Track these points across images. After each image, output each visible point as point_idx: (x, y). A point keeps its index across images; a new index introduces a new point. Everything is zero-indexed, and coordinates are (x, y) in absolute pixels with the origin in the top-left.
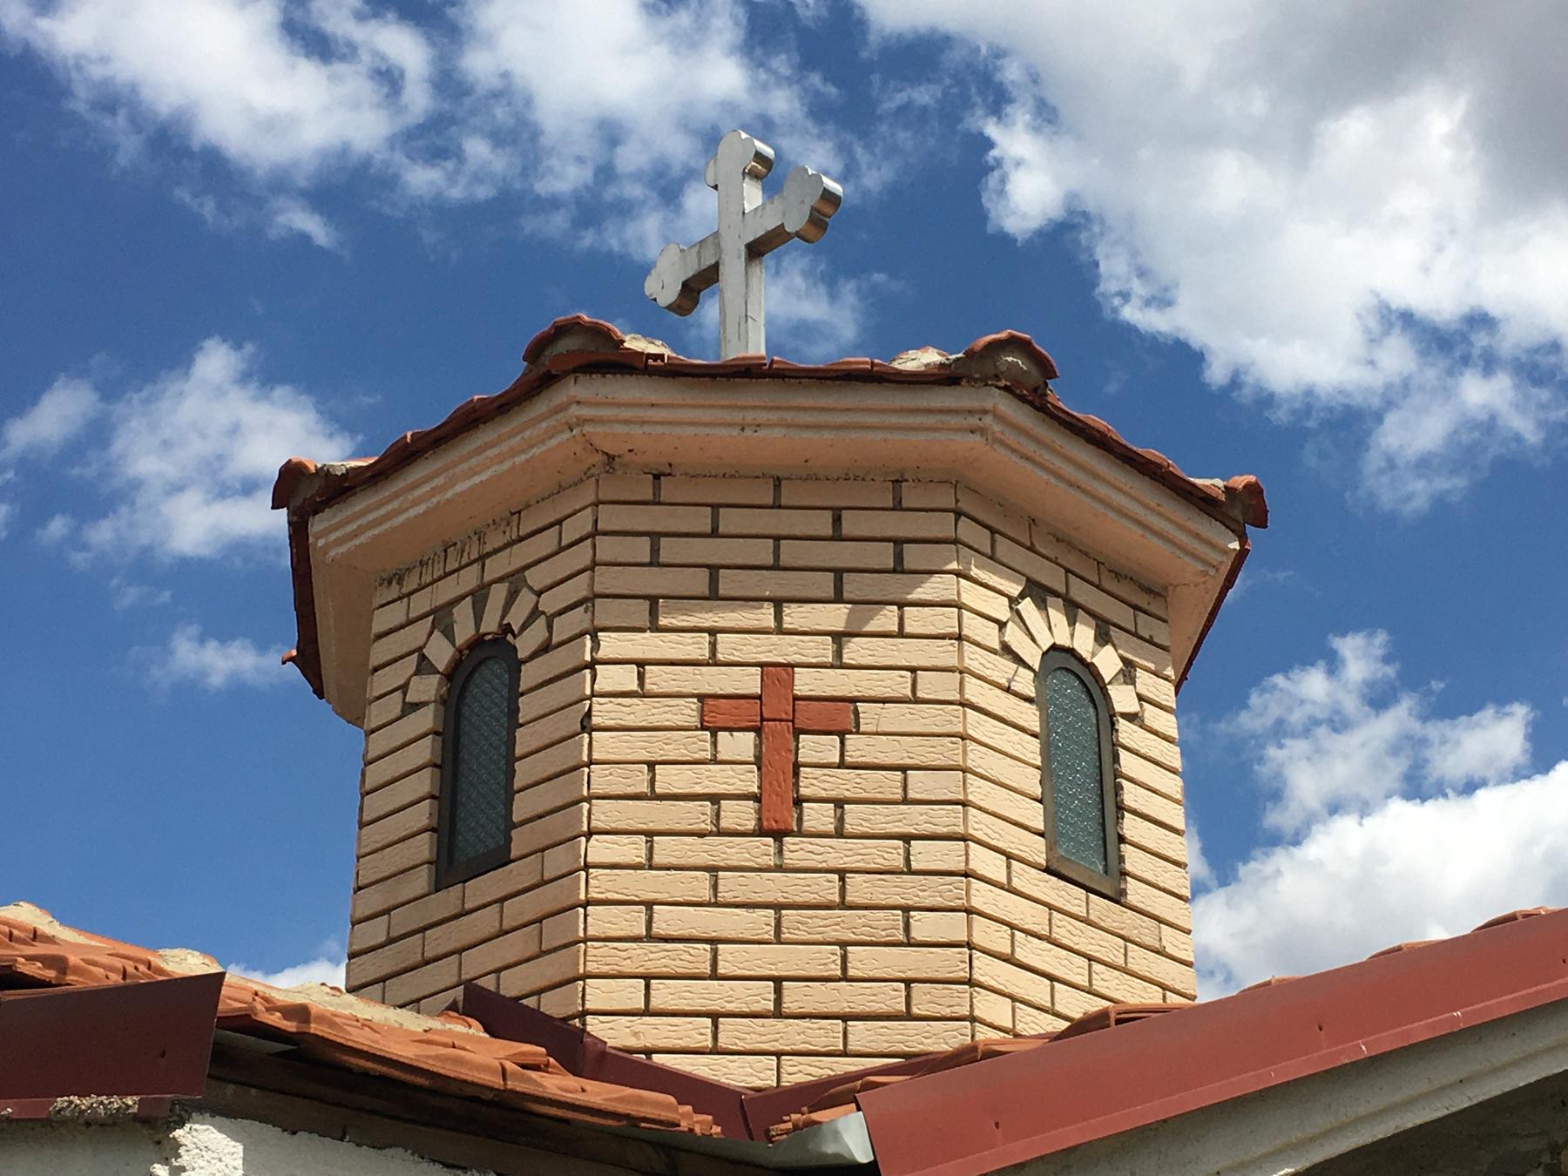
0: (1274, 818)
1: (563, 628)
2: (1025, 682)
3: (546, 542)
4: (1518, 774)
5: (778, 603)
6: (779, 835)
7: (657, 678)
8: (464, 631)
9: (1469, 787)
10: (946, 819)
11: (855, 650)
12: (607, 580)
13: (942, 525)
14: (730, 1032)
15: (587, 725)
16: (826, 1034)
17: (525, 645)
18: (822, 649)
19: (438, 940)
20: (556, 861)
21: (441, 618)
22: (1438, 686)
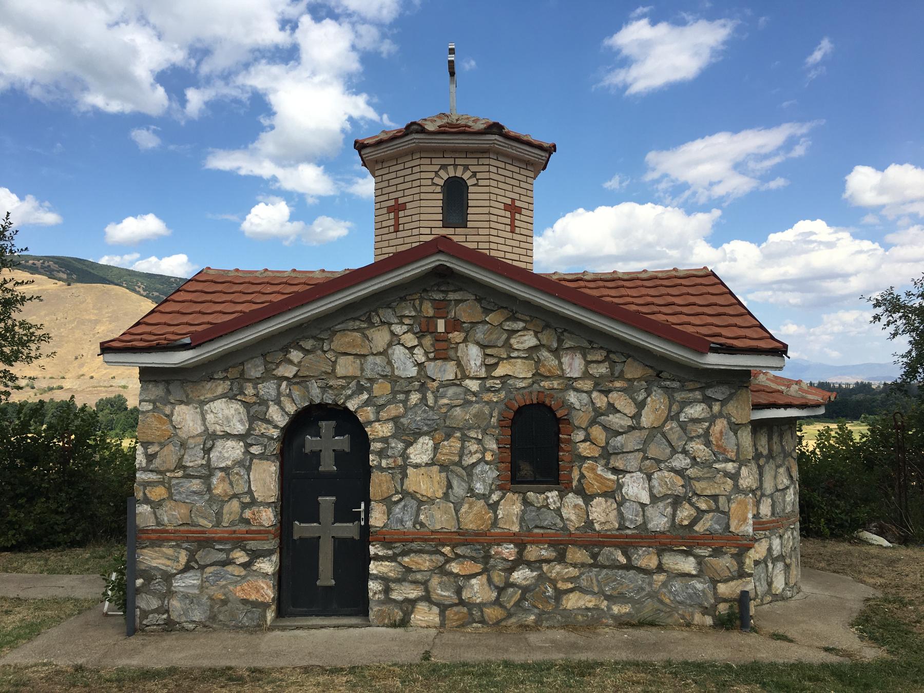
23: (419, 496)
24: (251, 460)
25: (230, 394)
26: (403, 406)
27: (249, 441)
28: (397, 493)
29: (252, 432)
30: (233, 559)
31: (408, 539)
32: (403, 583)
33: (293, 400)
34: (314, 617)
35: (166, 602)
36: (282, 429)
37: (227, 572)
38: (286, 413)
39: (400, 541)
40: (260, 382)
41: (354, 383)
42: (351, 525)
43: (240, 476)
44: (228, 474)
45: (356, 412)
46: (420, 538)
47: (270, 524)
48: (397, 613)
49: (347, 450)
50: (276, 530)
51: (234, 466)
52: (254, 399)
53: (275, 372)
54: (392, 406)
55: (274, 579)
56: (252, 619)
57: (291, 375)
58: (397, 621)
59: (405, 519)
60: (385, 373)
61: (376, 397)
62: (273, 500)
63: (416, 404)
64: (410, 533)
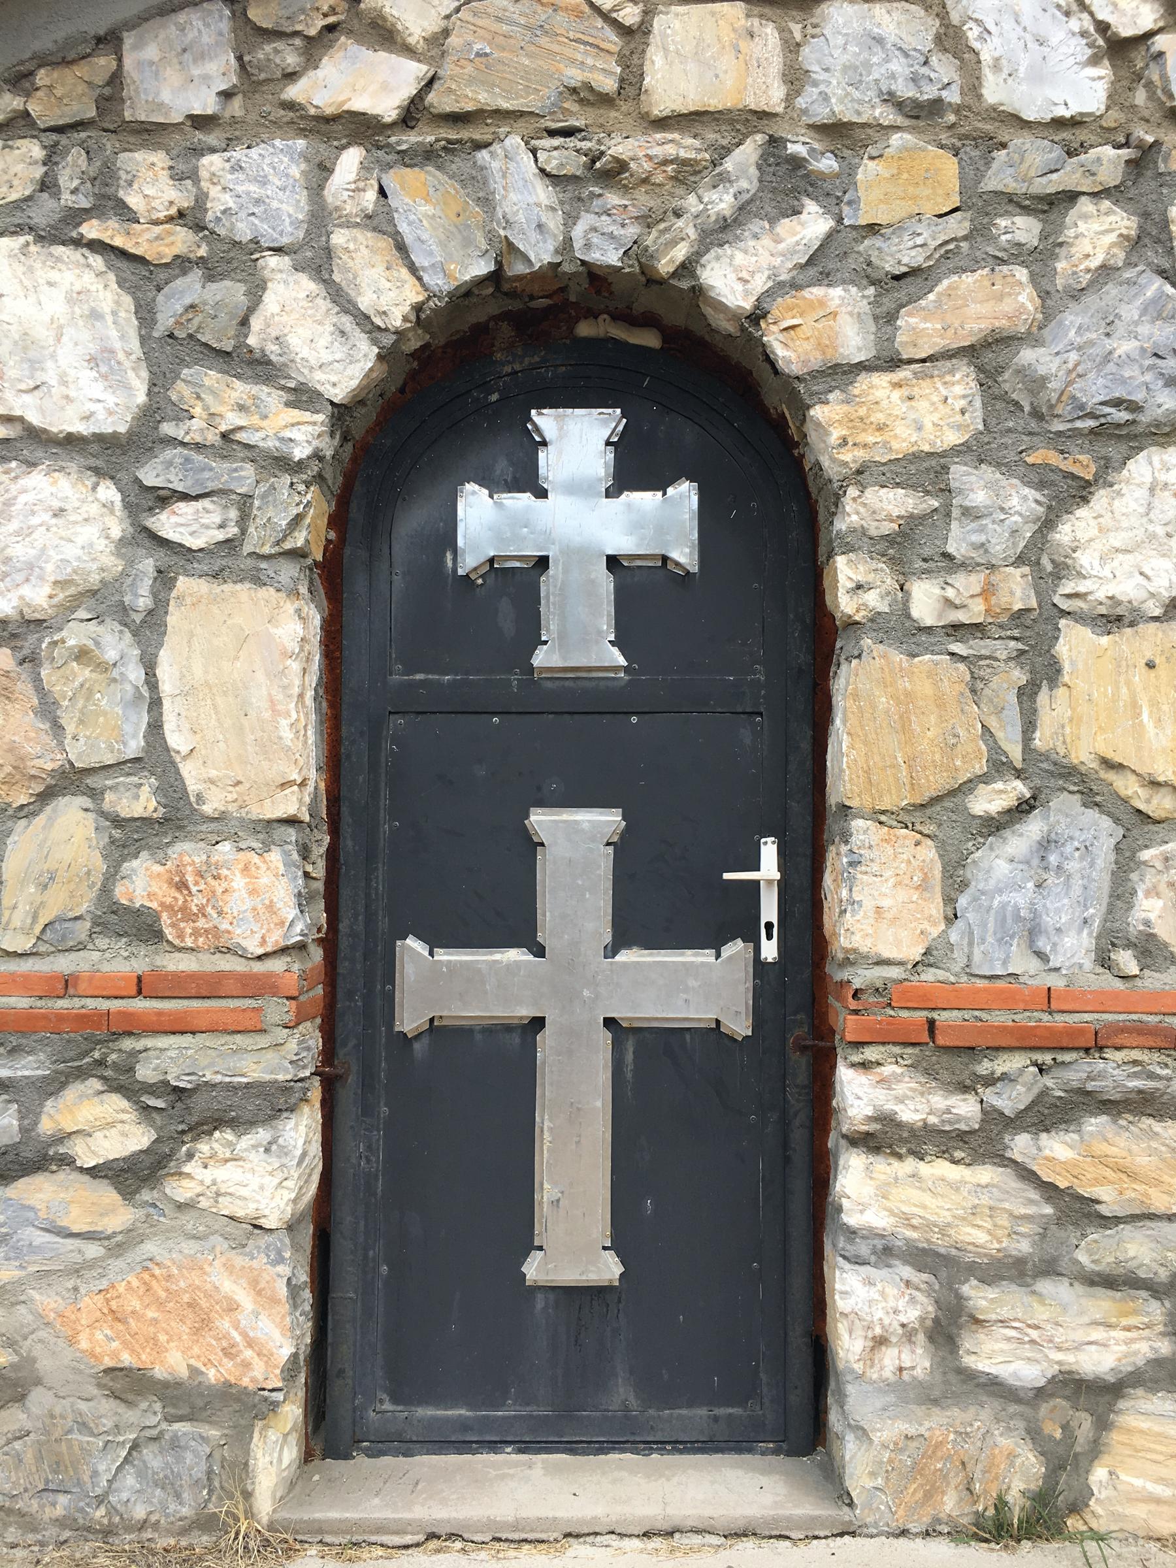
23: (1128, 786)
24: (164, 579)
25: (45, 212)
26: (1034, 279)
27: (150, 476)
28: (999, 767)
29: (168, 429)
30: (63, 1137)
31: (1074, 1032)
32: (1045, 1286)
33: (401, 248)
34: (508, 1458)
36: (341, 413)
37: (25, 1214)
38: (363, 320)
39: (1025, 1041)
40: (212, 139)
41: (747, 153)
42: (705, 957)
43: (103, 667)
44: (31, 660)
45: (757, 316)
46: (1141, 1030)
47: (276, 939)
48: (1012, 1456)
49: (685, 555)
50: (304, 976)
51: (67, 610)
52: (181, 240)
53: (294, 92)
54: (968, 279)
55: (296, 1247)
56: (169, 1484)
57: (387, 107)
58: (1014, 1498)
59: (1048, 921)
60: (930, 92)
61: (873, 229)
62: (291, 804)
63: (1105, 271)
64: (1076, 1000)
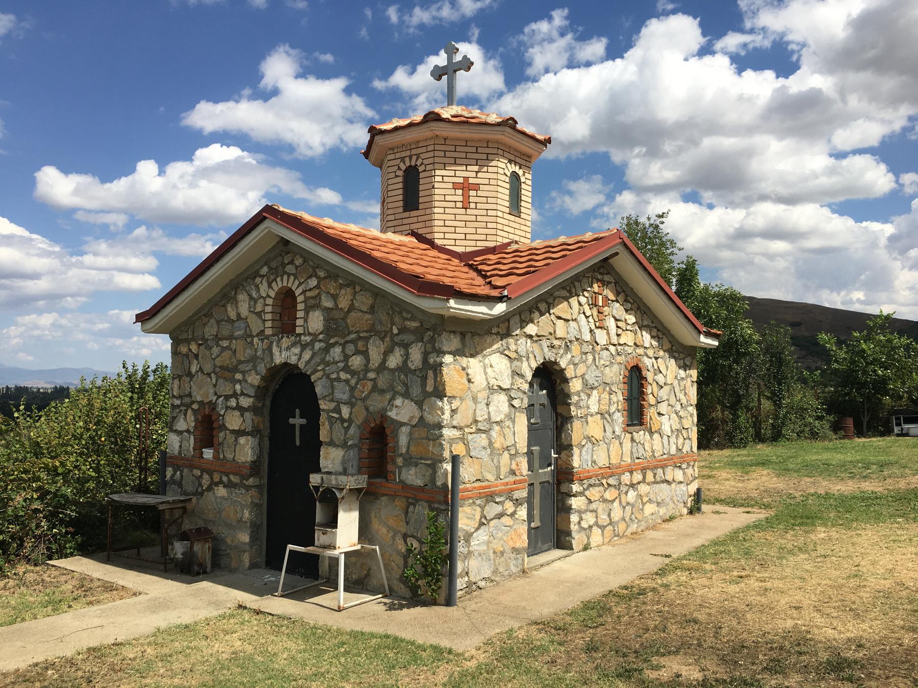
0: (530, 72)
1: (428, 168)
2: (507, 180)
3: (424, 149)
4: (603, 60)
5: (466, 165)
6: (466, 209)
7: (446, 179)
8: (408, 164)
9: (588, 64)
10: (494, 207)
11: (480, 175)
12: (437, 160)
13: (495, 151)
14: (458, 242)
15: (433, 187)
16: (473, 243)
17: (421, 169)
18: (474, 174)
19: (405, 221)
20: (428, 211)
21: (403, 159)
22: (580, 28)
35: (467, 563)
